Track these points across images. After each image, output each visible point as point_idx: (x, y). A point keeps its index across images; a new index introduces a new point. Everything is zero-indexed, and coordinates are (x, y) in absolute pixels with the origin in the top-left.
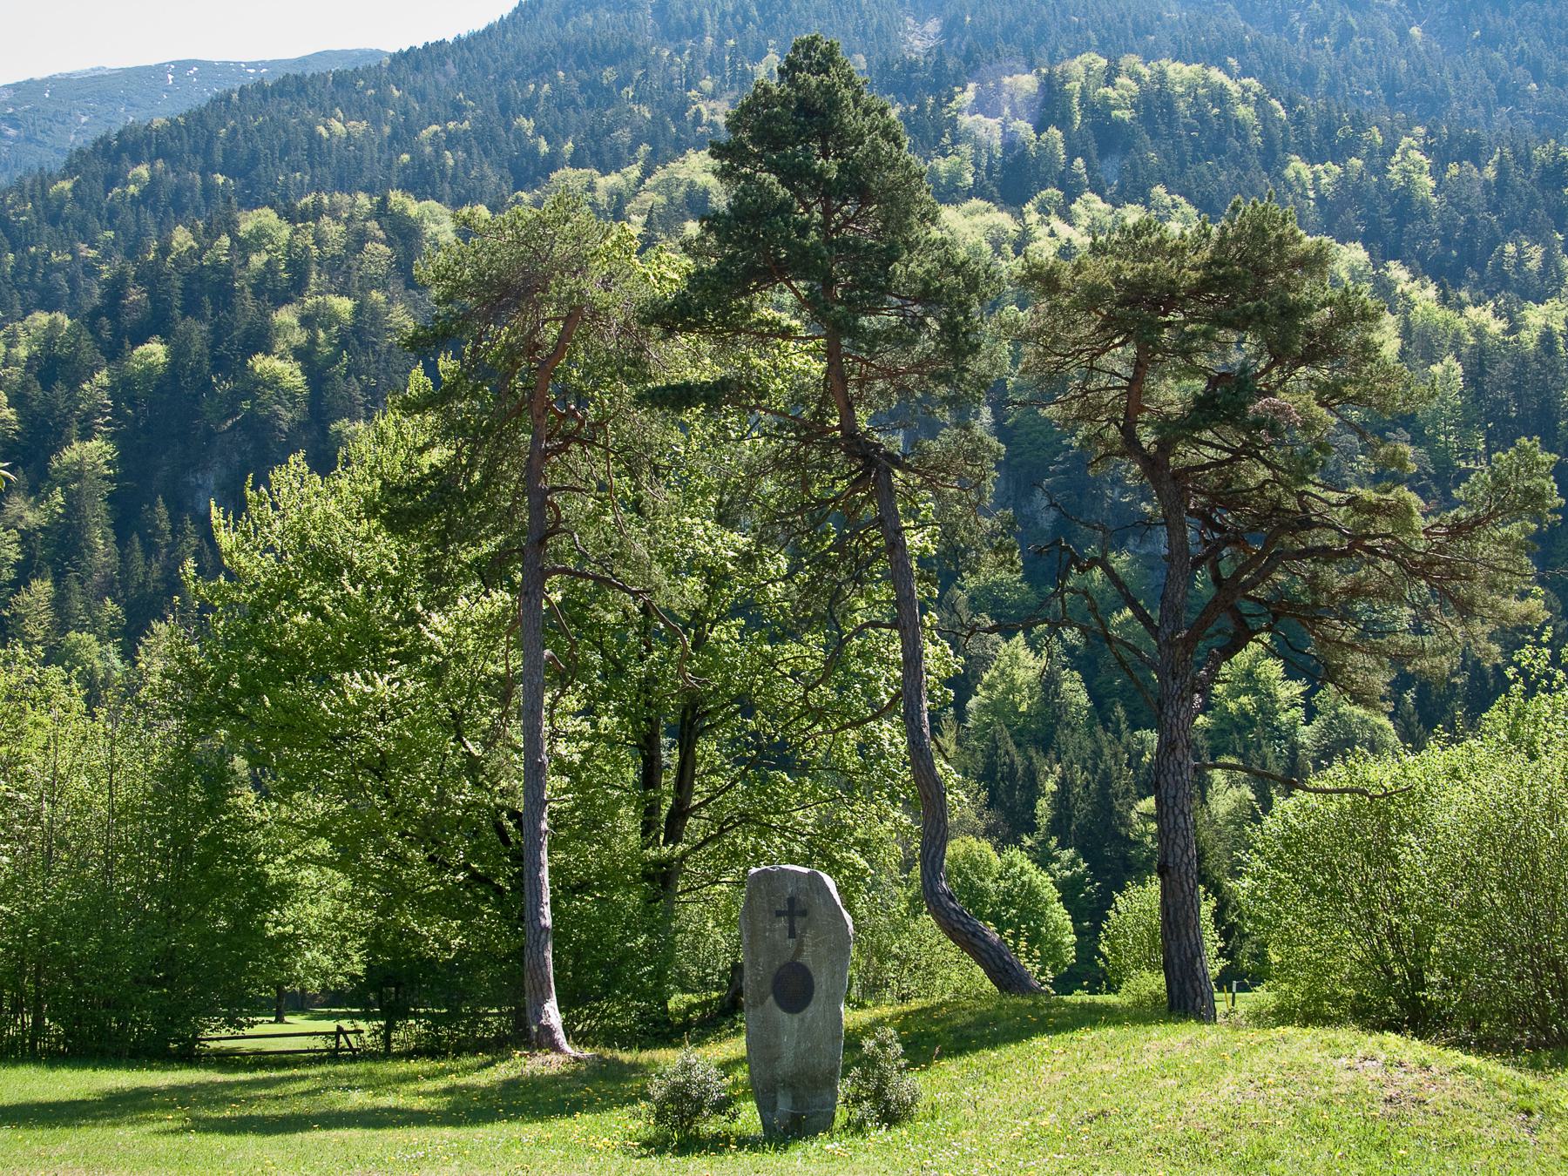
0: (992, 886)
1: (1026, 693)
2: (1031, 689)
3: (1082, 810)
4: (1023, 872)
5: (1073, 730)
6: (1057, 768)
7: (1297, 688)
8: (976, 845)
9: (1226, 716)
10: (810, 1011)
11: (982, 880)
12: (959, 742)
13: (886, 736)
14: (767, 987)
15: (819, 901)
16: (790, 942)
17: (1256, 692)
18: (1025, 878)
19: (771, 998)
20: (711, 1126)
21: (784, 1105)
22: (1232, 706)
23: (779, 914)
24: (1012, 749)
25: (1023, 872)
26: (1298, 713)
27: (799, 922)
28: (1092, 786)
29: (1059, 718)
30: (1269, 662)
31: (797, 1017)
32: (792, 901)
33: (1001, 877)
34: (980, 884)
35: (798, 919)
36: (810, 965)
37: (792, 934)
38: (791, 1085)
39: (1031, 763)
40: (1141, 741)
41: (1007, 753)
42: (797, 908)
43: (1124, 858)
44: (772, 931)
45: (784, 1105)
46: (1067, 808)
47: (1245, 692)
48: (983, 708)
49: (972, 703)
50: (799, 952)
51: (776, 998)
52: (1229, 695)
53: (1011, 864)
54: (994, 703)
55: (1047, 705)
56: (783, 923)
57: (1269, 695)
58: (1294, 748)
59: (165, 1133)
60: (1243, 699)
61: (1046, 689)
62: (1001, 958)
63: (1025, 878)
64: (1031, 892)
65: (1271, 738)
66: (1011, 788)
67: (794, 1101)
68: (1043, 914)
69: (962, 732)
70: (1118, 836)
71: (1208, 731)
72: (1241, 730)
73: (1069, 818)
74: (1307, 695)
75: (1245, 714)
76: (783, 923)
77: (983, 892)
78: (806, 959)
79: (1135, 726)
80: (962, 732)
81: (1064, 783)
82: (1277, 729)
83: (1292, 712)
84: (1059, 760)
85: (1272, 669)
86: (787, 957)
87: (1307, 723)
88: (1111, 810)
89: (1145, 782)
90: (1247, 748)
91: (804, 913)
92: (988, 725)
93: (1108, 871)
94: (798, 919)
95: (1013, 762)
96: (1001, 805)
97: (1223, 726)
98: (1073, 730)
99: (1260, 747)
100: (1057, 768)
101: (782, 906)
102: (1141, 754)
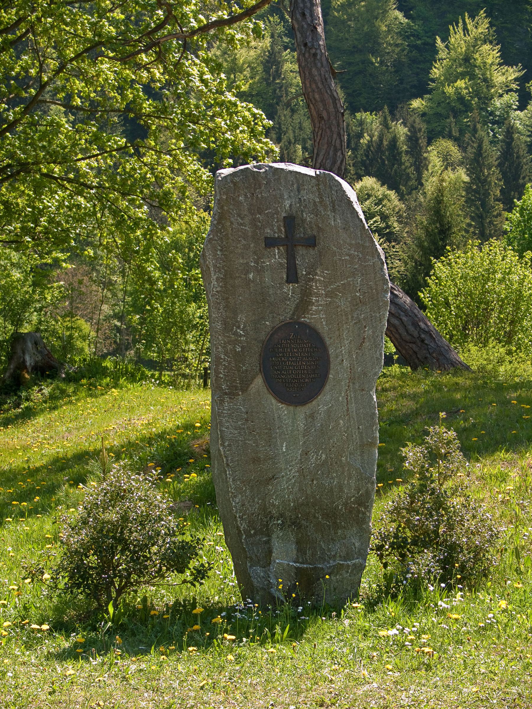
1: (247, 73)
2: (252, 69)
5: (293, 111)
7: (512, 73)
10: (322, 403)
13: (195, 71)
14: (252, 361)
15: (335, 221)
16: (289, 289)
17: (472, 77)
19: (259, 381)
20: (163, 592)
21: (284, 555)
22: (449, 90)
23: (270, 243)
26: (512, 99)
27: (304, 257)
29: (279, 98)
30: (487, 47)
31: (302, 412)
32: (290, 221)
35: (301, 251)
36: (323, 328)
37: (292, 276)
38: (295, 523)
40: (361, 123)
42: (300, 234)
44: (260, 271)
45: (284, 555)
47: (462, 76)
50: (304, 305)
51: (269, 382)
52: (446, 79)
55: (268, 84)
56: (277, 257)
57: (485, 80)
58: (510, 131)
60: (461, 83)
61: (267, 70)
62: (416, 325)
65: (485, 123)
67: (301, 550)
71: (424, 115)
72: (456, 113)
74: (522, 81)
75: (461, 99)
76: (277, 257)
78: (316, 316)
79: (354, 109)
82: (492, 113)
83: (506, 97)
85: (490, 54)
86: (285, 314)
87: (522, 107)
89: (363, 163)
90: (462, 132)
91: (311, 242)
94: (301, 251)
97: (439, 110)
98: (293, 111)
99: (475, 130)
101: (275, 230)
102: (360, 136)
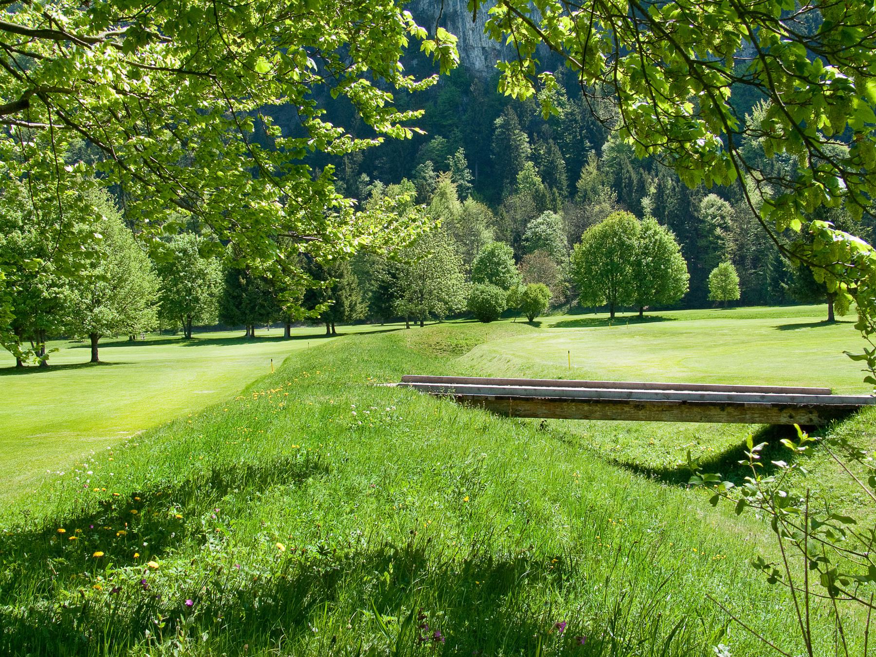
0: (636, 243)
3: (672, 203)
4: (656, 233)
6: (656, 180)
8: (626, 217)
9: (751, 150)
11: (630, 239)
12: (598, 169)
18: (656, 237)
24: (631, 169)
25: (656, 233)
28: (677, 189)
33: (641, 237)
34: (628, 242)
39: (642, 177)
41: (628, 171)
43: (696, 229)
46: (662, 202)
48: (612, 149)
49: (605, 147)
53: (648, 229)
54: (617, 146)
59: (559, 325)
60: (762, 139)
63: (656, 237)
64: (661, 246)
66: (631, 191)
68: (669, 260)
69: (600, 163)
70: (692, 217)
73: (664, 208)
77: (630, 247)
80: (600, 163)
81: (660, 188)
84: (657, 176)
88: (689, 202)
92: (614, 159)
93: (687, 238)
95: (630, 177)
96: (625, 201)
97: (749, 155)
100: (656, 180)
